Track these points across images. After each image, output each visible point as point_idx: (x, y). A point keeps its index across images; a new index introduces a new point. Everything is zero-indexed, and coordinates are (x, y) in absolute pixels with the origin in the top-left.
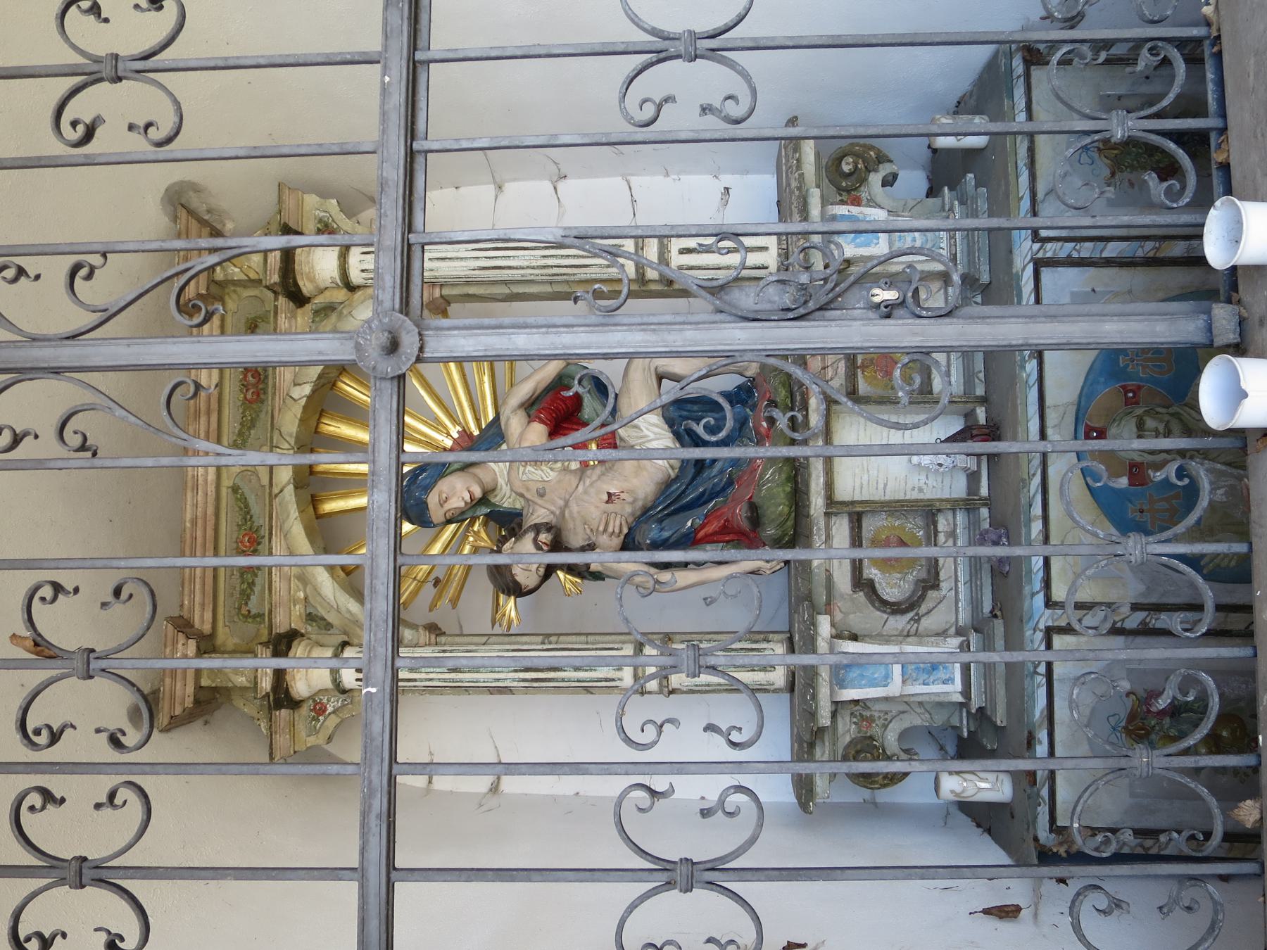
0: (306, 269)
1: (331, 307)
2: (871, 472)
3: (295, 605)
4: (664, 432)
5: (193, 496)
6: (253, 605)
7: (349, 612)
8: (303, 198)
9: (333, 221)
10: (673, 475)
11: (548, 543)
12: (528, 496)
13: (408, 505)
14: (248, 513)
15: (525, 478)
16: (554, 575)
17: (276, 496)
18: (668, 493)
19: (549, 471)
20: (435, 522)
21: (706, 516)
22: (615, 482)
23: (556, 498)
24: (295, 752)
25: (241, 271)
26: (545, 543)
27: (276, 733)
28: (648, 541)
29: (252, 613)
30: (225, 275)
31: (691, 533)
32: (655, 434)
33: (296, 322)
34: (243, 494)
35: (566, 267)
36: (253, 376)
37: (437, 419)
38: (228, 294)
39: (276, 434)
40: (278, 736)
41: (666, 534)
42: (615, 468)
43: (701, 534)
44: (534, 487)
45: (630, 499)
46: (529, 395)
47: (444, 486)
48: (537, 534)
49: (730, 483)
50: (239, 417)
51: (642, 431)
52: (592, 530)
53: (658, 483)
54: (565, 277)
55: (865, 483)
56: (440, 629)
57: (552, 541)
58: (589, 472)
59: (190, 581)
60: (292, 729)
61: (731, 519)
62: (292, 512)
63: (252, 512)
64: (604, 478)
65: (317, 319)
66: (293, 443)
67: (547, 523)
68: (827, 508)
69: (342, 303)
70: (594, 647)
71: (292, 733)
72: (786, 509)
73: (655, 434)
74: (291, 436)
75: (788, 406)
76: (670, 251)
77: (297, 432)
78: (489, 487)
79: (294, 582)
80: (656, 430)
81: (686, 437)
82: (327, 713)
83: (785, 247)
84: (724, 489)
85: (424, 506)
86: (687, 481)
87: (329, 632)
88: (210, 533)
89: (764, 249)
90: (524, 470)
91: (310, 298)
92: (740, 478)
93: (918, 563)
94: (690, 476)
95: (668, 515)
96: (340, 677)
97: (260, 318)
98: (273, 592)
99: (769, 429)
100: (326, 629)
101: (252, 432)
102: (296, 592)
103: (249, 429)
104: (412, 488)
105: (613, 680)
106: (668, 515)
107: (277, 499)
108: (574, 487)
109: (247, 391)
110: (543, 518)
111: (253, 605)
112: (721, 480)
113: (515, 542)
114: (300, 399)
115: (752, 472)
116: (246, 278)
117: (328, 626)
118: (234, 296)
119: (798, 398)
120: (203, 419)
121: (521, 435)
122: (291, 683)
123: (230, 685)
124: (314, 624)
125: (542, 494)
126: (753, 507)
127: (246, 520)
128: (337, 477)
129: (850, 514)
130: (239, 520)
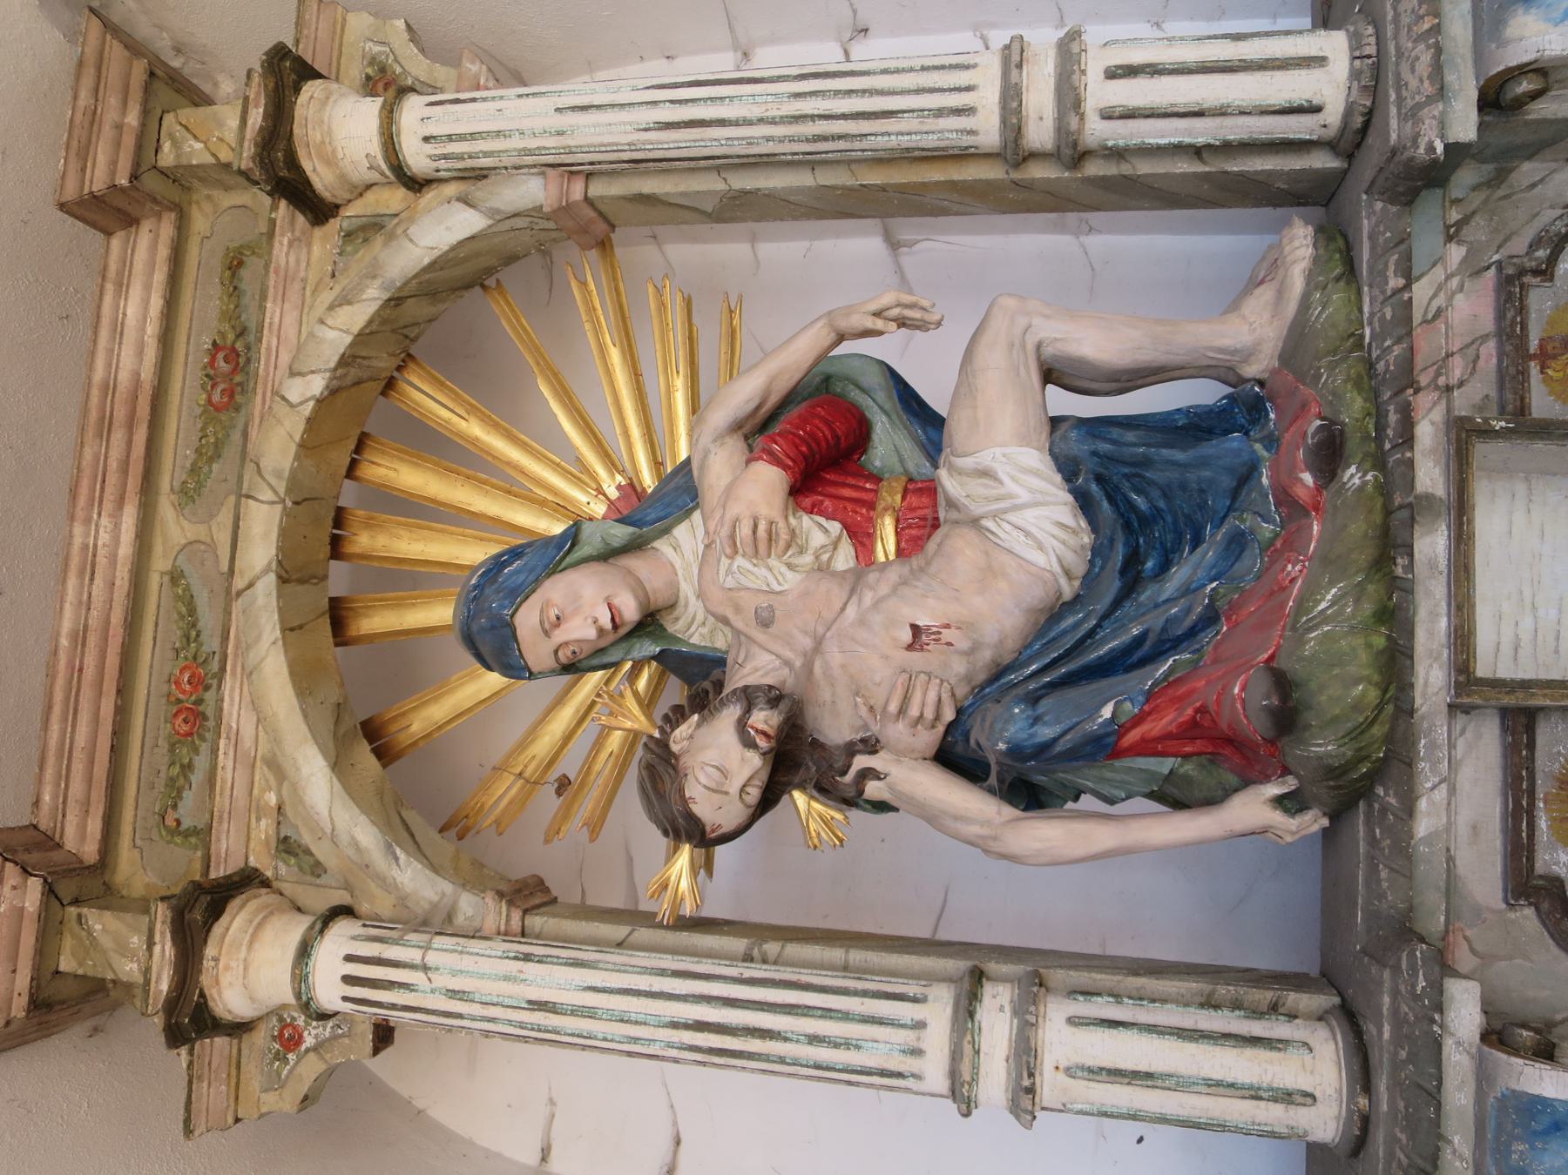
0: (315, 136)
1: (375, 224)
2: (1541, 613)
3: (258, 819)
4: (1053, 490)
5: (82, 585)
6: (188, 811)
7: (355, 844)
8: (344, 20)
9: (396, 60)
10: (1068, 592)
11: (771, 732)
12: (738, 623)
13: (475, 628)
14: (194, 625)
15: (730, 582)
16: (785, 798)
17: (239, 594)
18: (1052, 634)
19: (784, 569)
20: (535, 669)
21: (1150, 696)
22: (931, 601)
23: (795, 631)
24: (237, 1120)
25: (207, 148)
26: (764, 733)
27: (200, 1078)
28: (1002, 746)
29: (184, 826)
30: (178, 156)
31: (1108, 735)
32: (1032, 491)
33: (309, 253)
34: (187, 588)
35: (844, 117)
36: (226, 360)
37: (580, 461)
38: (197, 202)
39: (250, 468)
40: (205, 1085)
41: (1046, 732)
42: (933, 569)
43: (1133, 736)
44: (750, 603)
45: (963, 644)
46: (752, 405)
48: (748, 711)
49: (1210, 618)
50: (195, 438)
51: (1001, 483)
52: (871, 709)
53: (1031, 611)
54: (841, 145)
55: (1526, 638)
56: (547, 890)
57: (780, 729)
58: (872, 577)
59: (60, 756)
60: (234, 1072)
61: (1212, 708)
62: (268, 628)
63: (200, 625)
64: (906, 590)
65: (349, 249)
66: (282, 491)
67: (771, 687)
68: (1458, 695)
69: (396, 215)
70: (860, 985)
71: (233, 1081)
72: (1373, 695)
73: (1032, 491)
74: (279, 476)
75: (1368, 433)
76: (1083, 72)
77: (293, 472)
78: (659, 598)
79: (261, 771)
80: (1036, 483)
81: (1105, 504)
82: (303, 1048)
83: (1371, 50)
84: (1192, 632)
85: (505, 632)
86: (1101, 606)
87: (318, 881)
88: (113, 660)
89: (1319, 61)
90: (730, 565)
91: (337, 207)
92: (1234, 607)
93: (218, 428)
94: (1107, 600)
95: (1053, 686)
96: (308, 988)
97: (249, 247)
98: (218, 788)
99: (1319, 488)
100: (313, 874)
101: (215, 466)
102: (263, 791)
103: (211, 460)
104: (488, 591)
105: (900, 1075)
106: (1053, 686)
107: (240, 600)
108: (838, 605)
109: (213, 387)
110: (767, 674)
111: (188, 811)
112: (1188, 611)
113: (699, 725)
114: (302, 403)
115: (1272, 593)
116: (214, 161)
117: (317, 869)
118: (207, 207)
119: (1393, 418)
120: (118, 436)
121: (729, 490)
122: (211, 993)
123: (110, 976)
124: (293, 861)
125: (765, 621)
126: (1282, 682)
127: (188, 640)
128: (387, 565)
129: (1505, 712)
130: (176, 638)
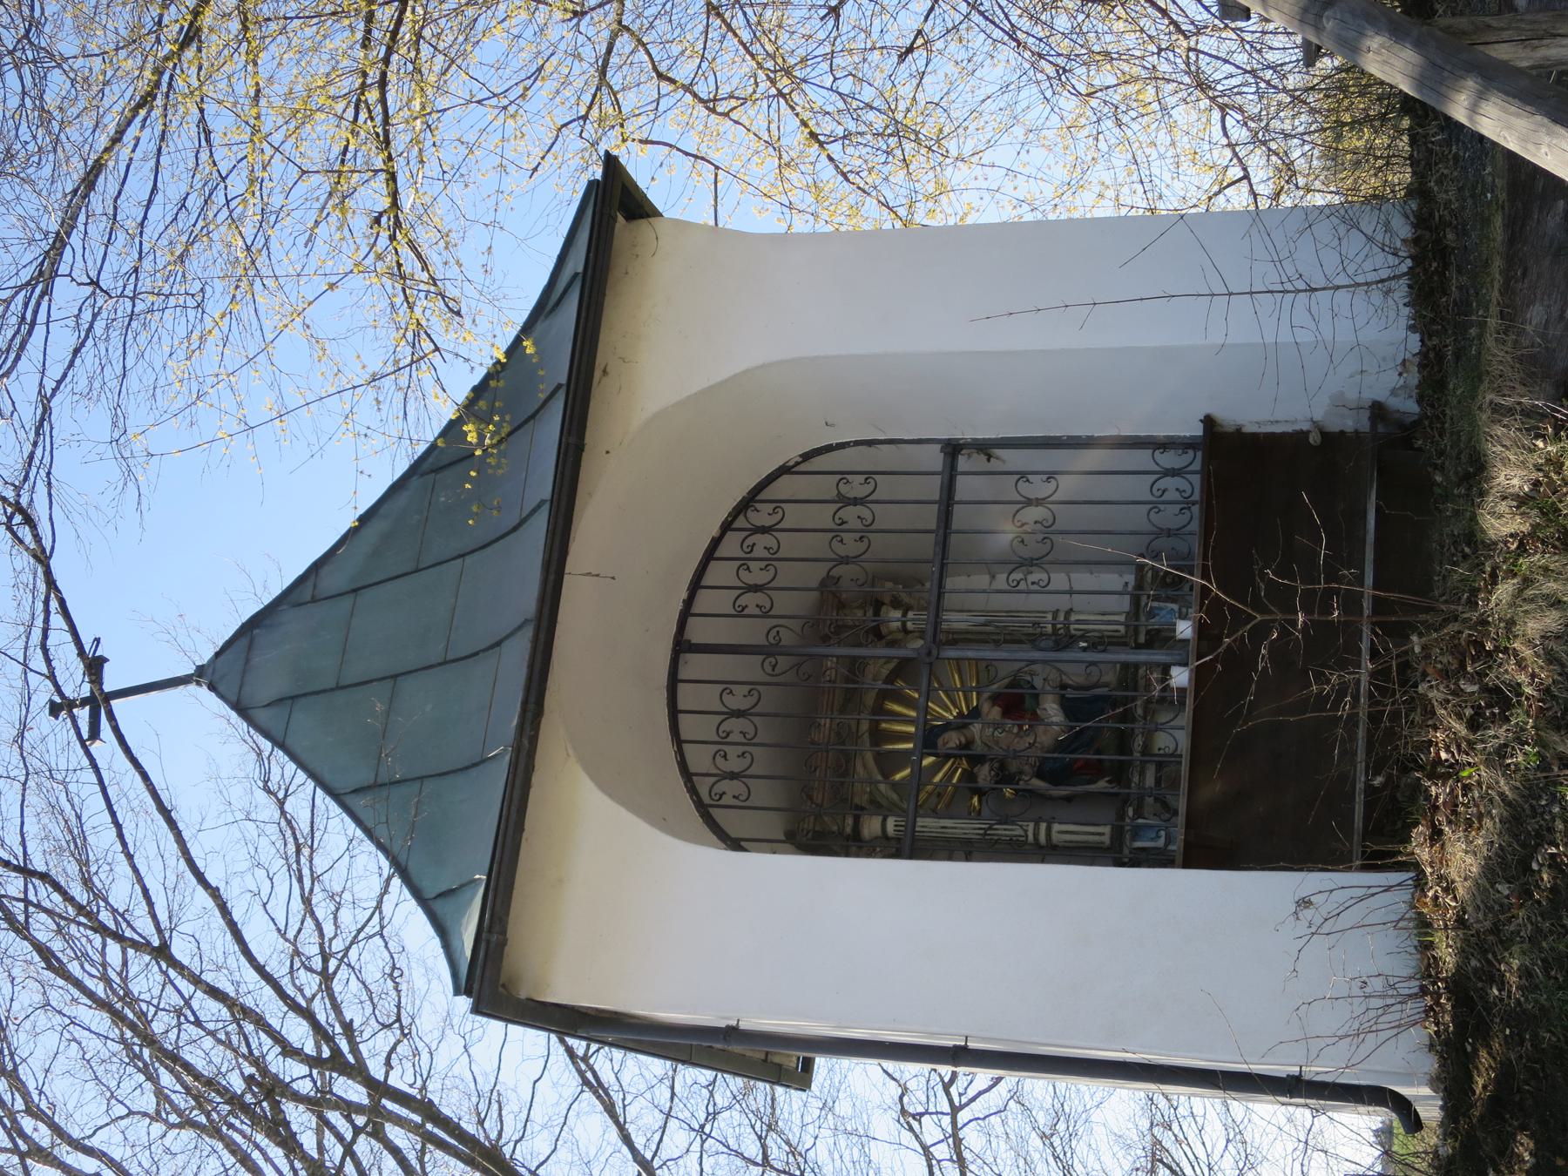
37: (946, 705)
47: (947, 736)
